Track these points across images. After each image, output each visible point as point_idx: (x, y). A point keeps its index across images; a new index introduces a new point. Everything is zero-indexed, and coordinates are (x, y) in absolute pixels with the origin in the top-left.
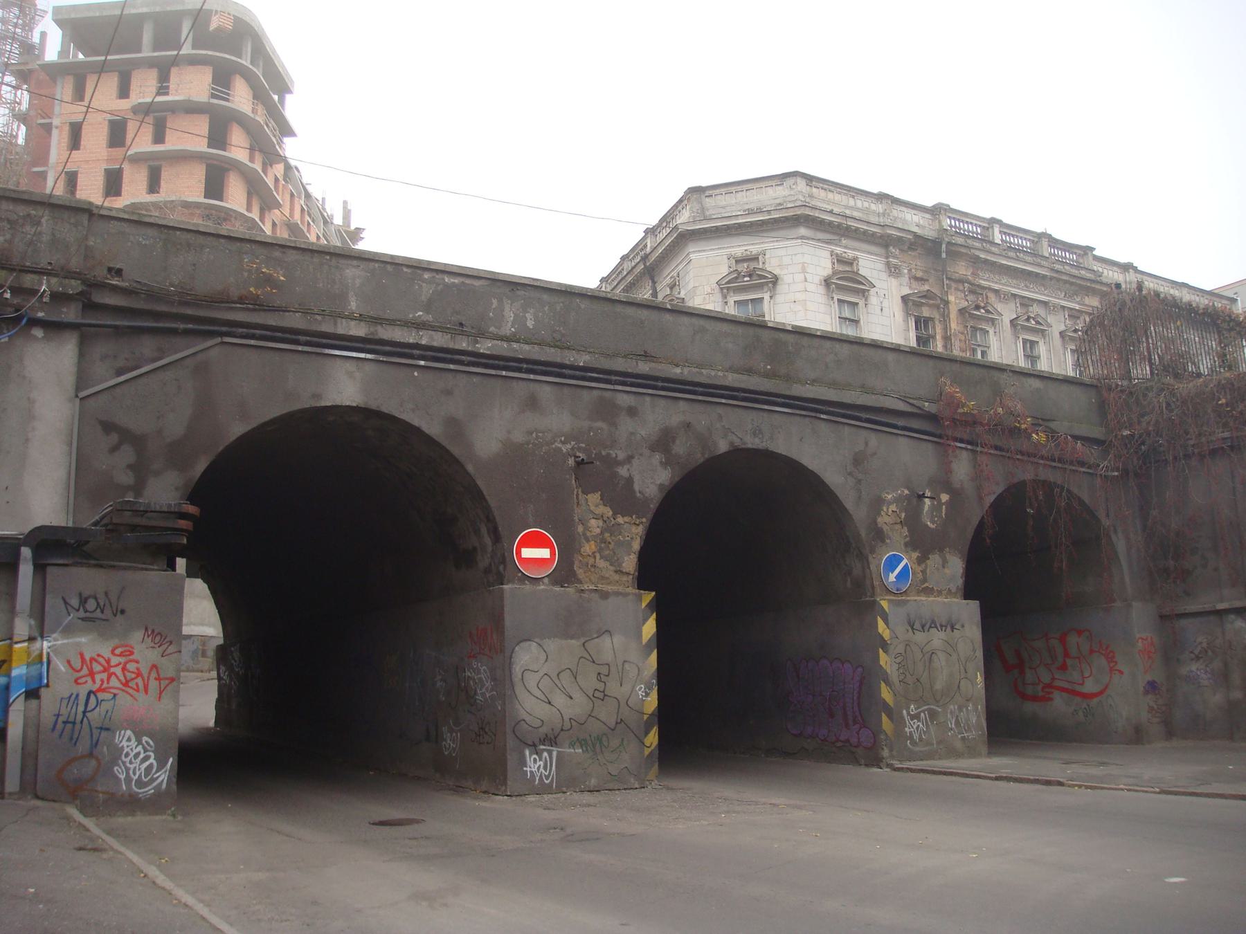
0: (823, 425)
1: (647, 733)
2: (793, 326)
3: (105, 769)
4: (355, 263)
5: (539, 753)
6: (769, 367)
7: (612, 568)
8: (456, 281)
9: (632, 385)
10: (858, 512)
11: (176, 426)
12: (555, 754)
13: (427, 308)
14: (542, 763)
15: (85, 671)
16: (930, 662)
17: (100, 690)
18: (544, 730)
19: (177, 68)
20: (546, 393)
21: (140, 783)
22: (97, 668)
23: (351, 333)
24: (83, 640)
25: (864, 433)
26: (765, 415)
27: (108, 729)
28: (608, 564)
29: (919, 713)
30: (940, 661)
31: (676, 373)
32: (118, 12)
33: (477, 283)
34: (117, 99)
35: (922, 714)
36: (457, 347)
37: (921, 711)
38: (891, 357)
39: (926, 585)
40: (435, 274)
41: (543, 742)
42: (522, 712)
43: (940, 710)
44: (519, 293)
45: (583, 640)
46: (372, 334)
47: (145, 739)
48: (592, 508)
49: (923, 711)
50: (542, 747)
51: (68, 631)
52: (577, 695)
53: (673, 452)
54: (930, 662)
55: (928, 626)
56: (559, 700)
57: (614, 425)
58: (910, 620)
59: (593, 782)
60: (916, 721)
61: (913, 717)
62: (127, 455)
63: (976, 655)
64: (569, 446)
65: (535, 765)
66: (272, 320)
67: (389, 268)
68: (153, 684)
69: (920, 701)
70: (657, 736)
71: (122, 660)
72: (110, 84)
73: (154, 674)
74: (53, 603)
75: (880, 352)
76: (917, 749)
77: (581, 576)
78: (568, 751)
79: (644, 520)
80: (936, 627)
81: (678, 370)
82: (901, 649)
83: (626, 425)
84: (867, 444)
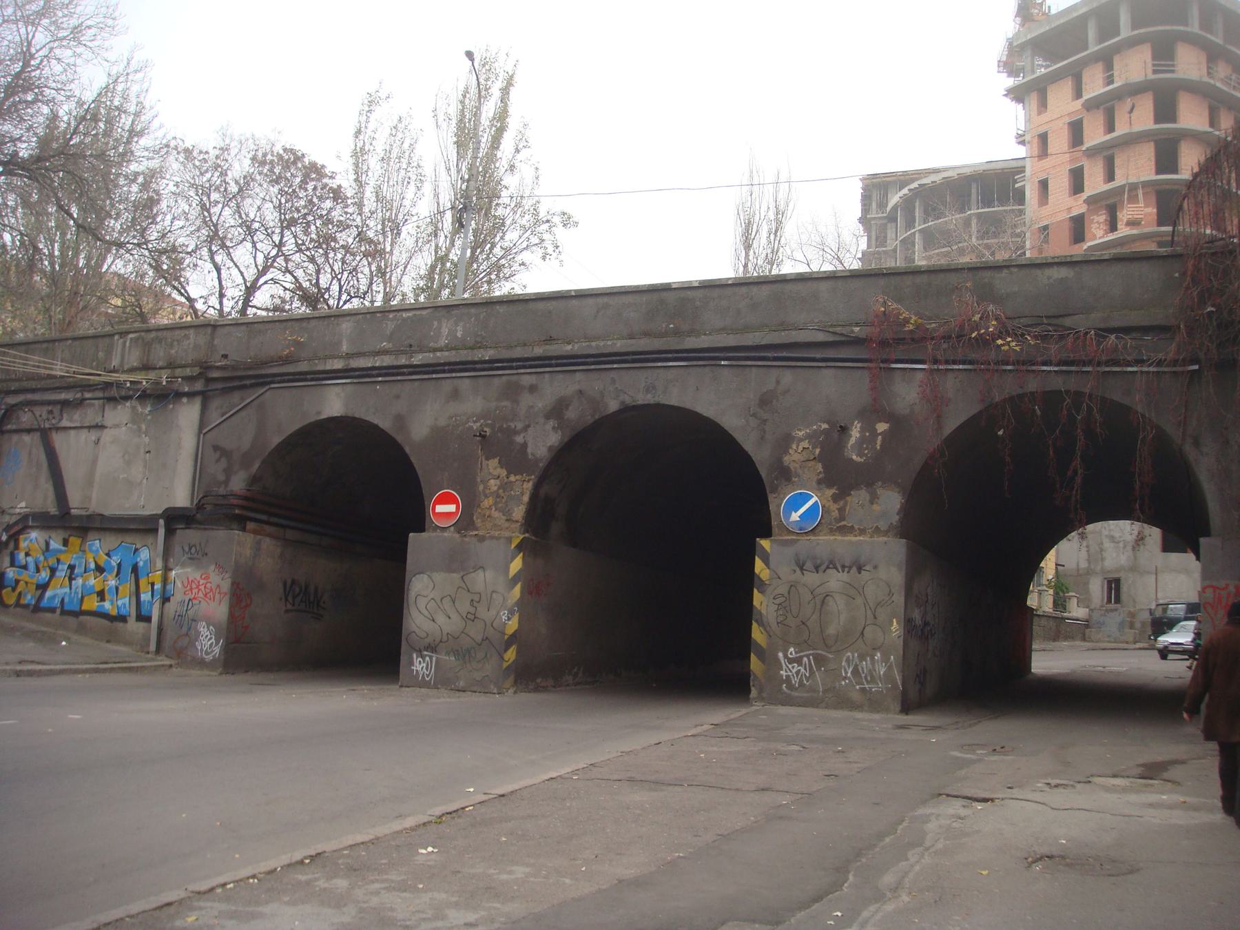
0: (726, 372)
1: (506, 650)
2: (700, 282)
3: (192, 643)
4: (348, 318)
5: (423, 657)
6: (672, 326)
7: (504, 518)
8: (410, 314)
9: (531, 367)
10: (760, 455)
11: (246, 443)
12: (434, 659)
13: (390, 339)
14: (425, 665)
15: (189, 588)
16: (822, 606)
17: (195, 598)
18: (427, 641)
19: (1118, 55)
20: (465, 385)
21: (207, 653)
22: (194, 586)
23: (334, 368)
24: (189, 570)
25: (775, 372)
26: (661, 371)
27: (195, 621)
28: (501, 514)
29: (801, 658)
30: (838, 605)
31: (567, 351)
32: (1018, 26)
33: (424, 312)
34: (1073, 100)
35: (805, 659)
36: (399, 363)
37: (804, 656)
38: (824, 286)
39: (843, 523)
40: (396, 313)
41: (426, 649)
42: (414, 625)
43: (831, 656)
44: (453, 312)
45: (462, 574)
46: (347, 365)
47: (211, 627)
48: (491, 471)
49: (808, 656)
50: (426, 653)
51: (183, 565)
52: (454, 616)
53: (566, 417)
54: (822, 606)
55: (823, 567)
56: (441, 619)
57: (516, 401)
58: (799, 560)
59: (462, 684)
60: (795, 665)
61: (791, 661)
62: (223, 463)
63: (893, 599)
64: (478, 424)
65: (420, 666)
66: (290, 369)
67: (368, 316)
68: (217, 596)
69: (802, 645)
70: (515, 652)
71: (205, 581)
72: (1067, 86)
73: (218, 590)
74: (177, 549)
75: (809, 284)
76: (795, 694)
77: (479, 525)
78: (445, 657)
79: (533, 477)
80: (836, 568)
81: (569, 347)
82: (783, 589)
83: (526, 400)
84: (778, 382)
